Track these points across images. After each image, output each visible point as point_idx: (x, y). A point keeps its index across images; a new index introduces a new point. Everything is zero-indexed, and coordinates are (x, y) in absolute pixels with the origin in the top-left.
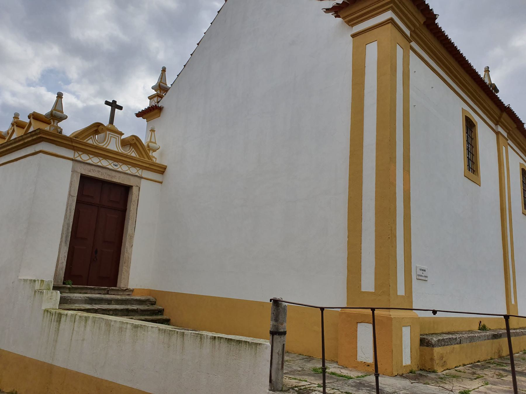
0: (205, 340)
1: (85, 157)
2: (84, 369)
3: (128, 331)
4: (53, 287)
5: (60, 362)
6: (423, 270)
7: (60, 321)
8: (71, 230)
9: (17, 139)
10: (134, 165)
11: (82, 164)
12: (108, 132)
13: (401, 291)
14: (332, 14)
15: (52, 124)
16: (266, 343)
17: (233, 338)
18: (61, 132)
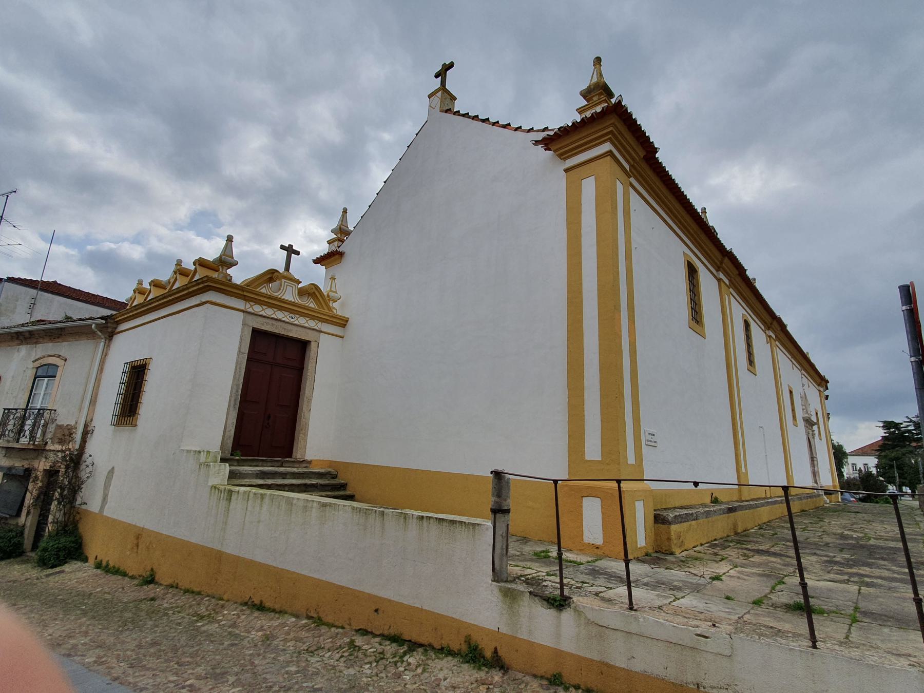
0: (411, 521)
1: (257, 309)
2: (260, 557)
3: (314, 510)
4: (221, 459)
5: (230, 548)
6: (652, 435)
7: (230, 499)
8: (240, 393)
9: (181, 289)
10: (313, 318)
11: (254, 317)
12: (283, 280)
13: (631, 460)
14: (542, 147)
15: (221, 270)
16: (487, 523)
17: (444, 518)
18: (230, 280)
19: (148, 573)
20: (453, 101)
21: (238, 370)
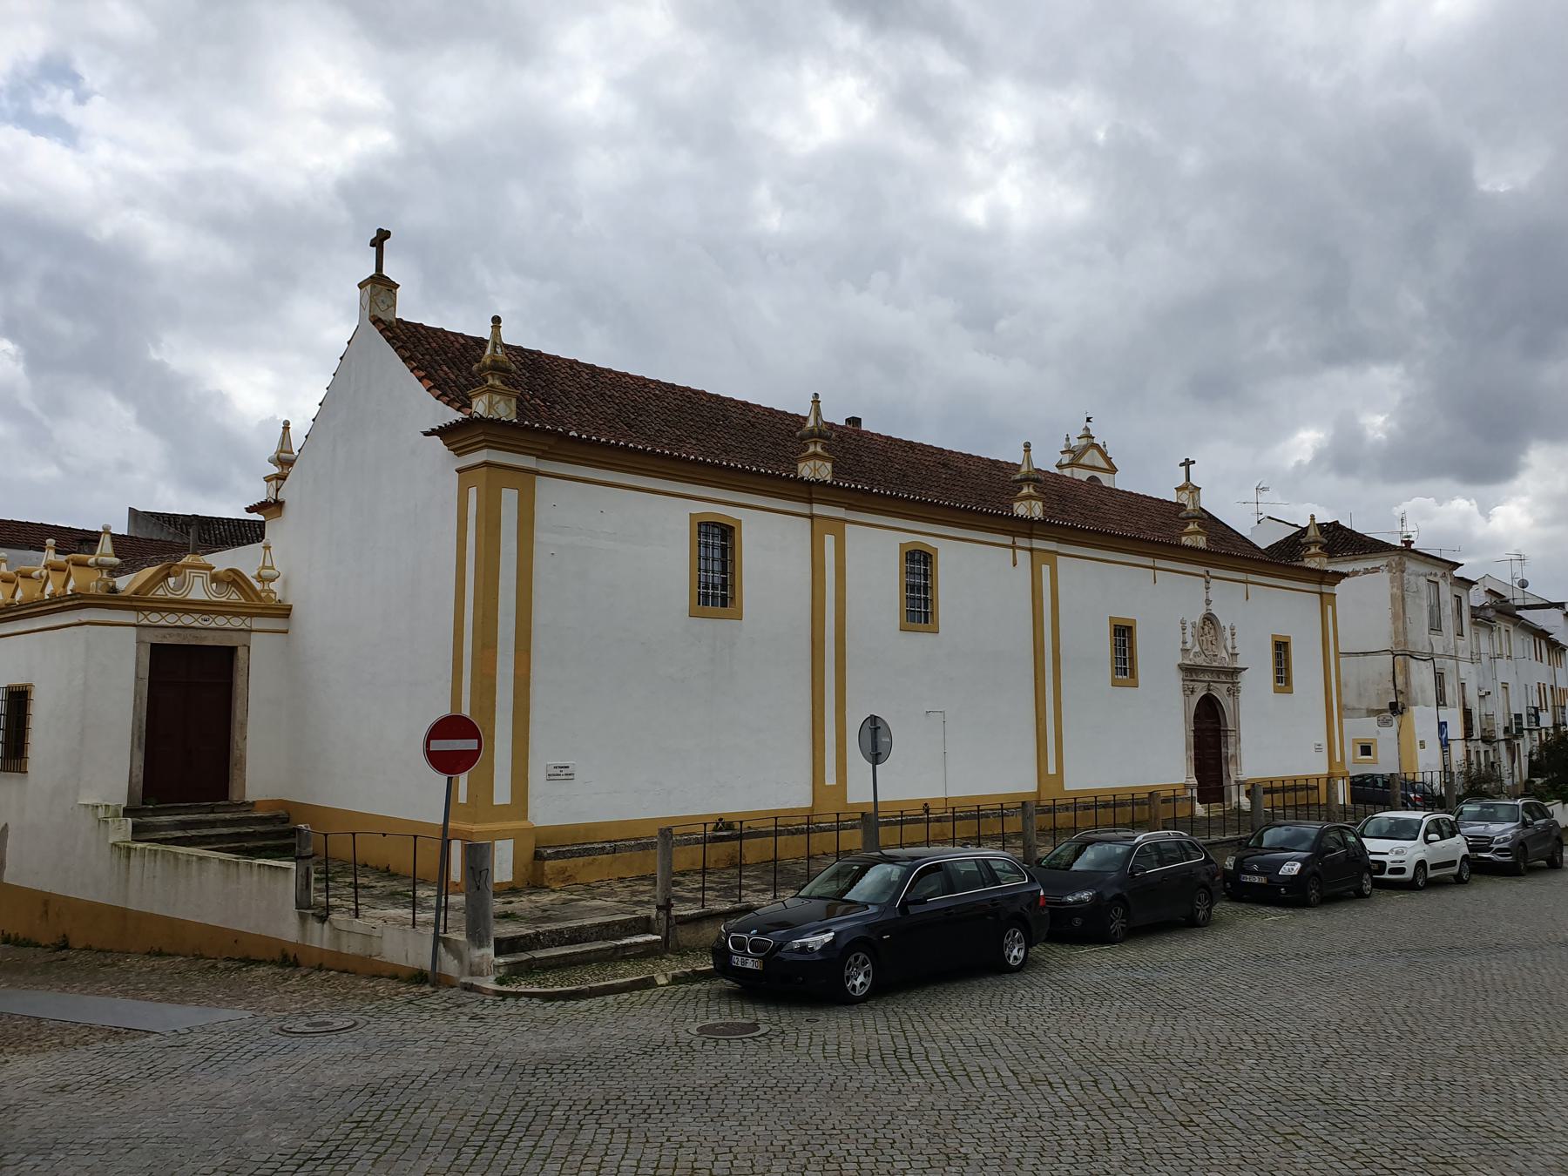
1: (154, 618)
5: (133, 906)
12: (188, 571)
19: (61, 939)
20: (394, 291)
21: (138, 701)
